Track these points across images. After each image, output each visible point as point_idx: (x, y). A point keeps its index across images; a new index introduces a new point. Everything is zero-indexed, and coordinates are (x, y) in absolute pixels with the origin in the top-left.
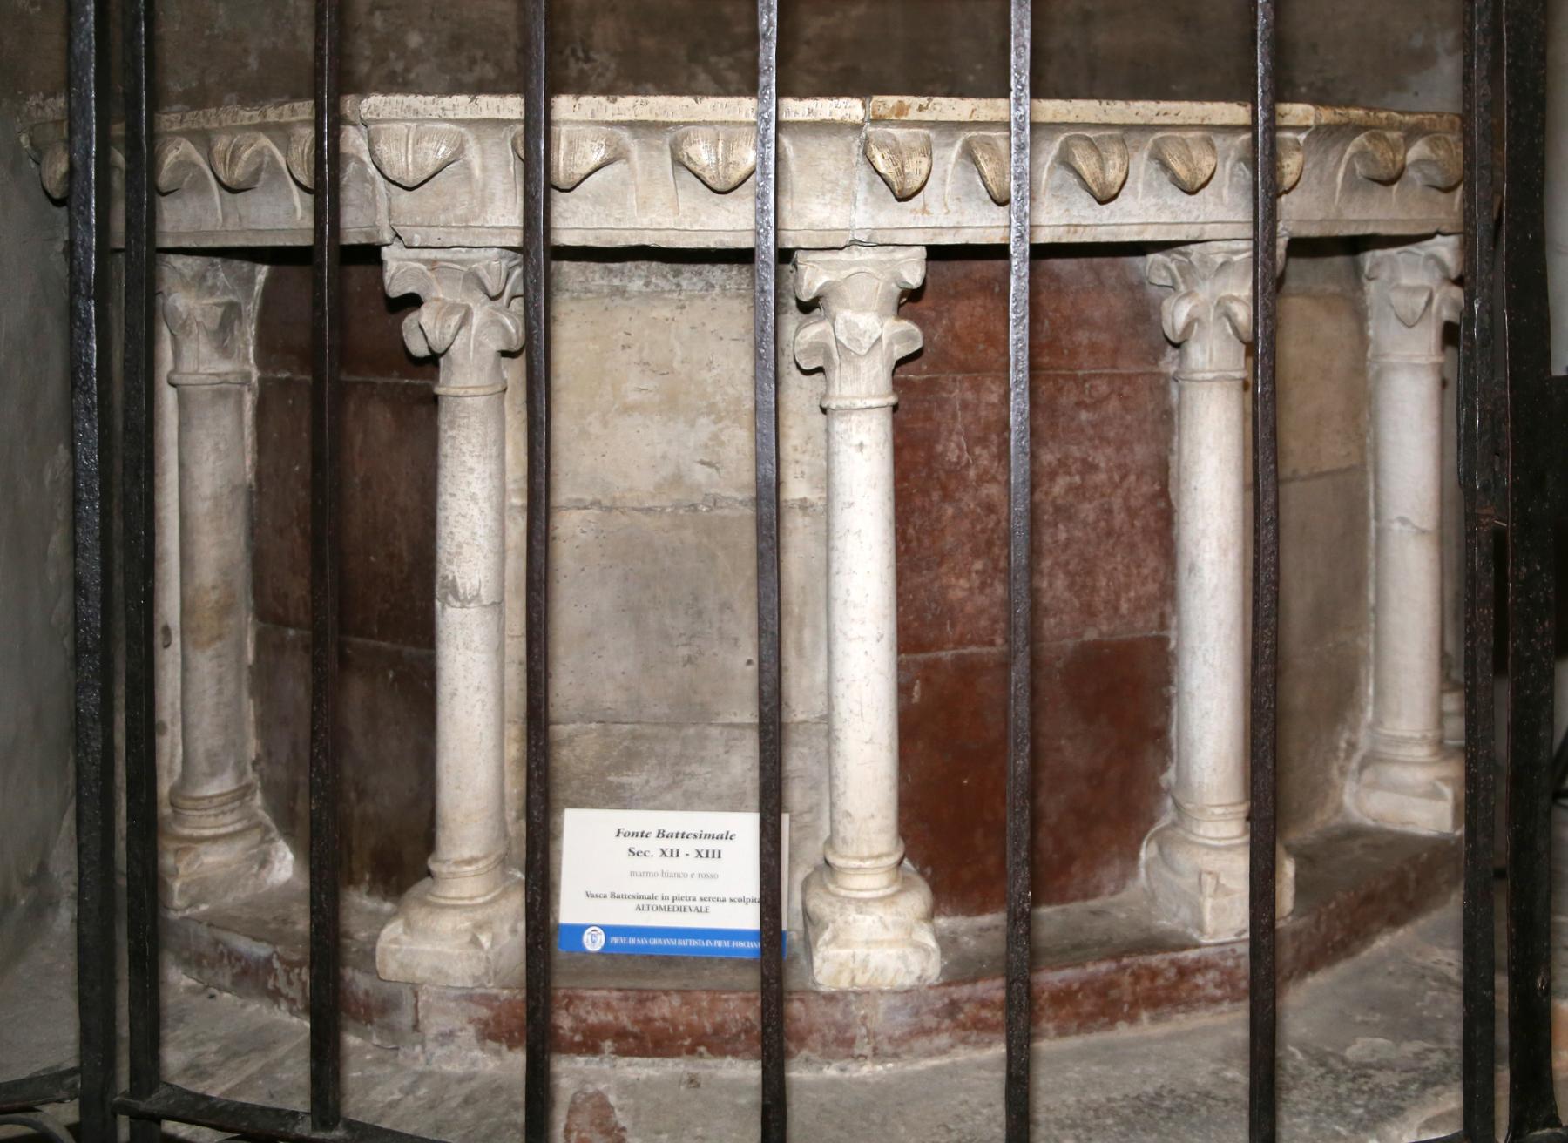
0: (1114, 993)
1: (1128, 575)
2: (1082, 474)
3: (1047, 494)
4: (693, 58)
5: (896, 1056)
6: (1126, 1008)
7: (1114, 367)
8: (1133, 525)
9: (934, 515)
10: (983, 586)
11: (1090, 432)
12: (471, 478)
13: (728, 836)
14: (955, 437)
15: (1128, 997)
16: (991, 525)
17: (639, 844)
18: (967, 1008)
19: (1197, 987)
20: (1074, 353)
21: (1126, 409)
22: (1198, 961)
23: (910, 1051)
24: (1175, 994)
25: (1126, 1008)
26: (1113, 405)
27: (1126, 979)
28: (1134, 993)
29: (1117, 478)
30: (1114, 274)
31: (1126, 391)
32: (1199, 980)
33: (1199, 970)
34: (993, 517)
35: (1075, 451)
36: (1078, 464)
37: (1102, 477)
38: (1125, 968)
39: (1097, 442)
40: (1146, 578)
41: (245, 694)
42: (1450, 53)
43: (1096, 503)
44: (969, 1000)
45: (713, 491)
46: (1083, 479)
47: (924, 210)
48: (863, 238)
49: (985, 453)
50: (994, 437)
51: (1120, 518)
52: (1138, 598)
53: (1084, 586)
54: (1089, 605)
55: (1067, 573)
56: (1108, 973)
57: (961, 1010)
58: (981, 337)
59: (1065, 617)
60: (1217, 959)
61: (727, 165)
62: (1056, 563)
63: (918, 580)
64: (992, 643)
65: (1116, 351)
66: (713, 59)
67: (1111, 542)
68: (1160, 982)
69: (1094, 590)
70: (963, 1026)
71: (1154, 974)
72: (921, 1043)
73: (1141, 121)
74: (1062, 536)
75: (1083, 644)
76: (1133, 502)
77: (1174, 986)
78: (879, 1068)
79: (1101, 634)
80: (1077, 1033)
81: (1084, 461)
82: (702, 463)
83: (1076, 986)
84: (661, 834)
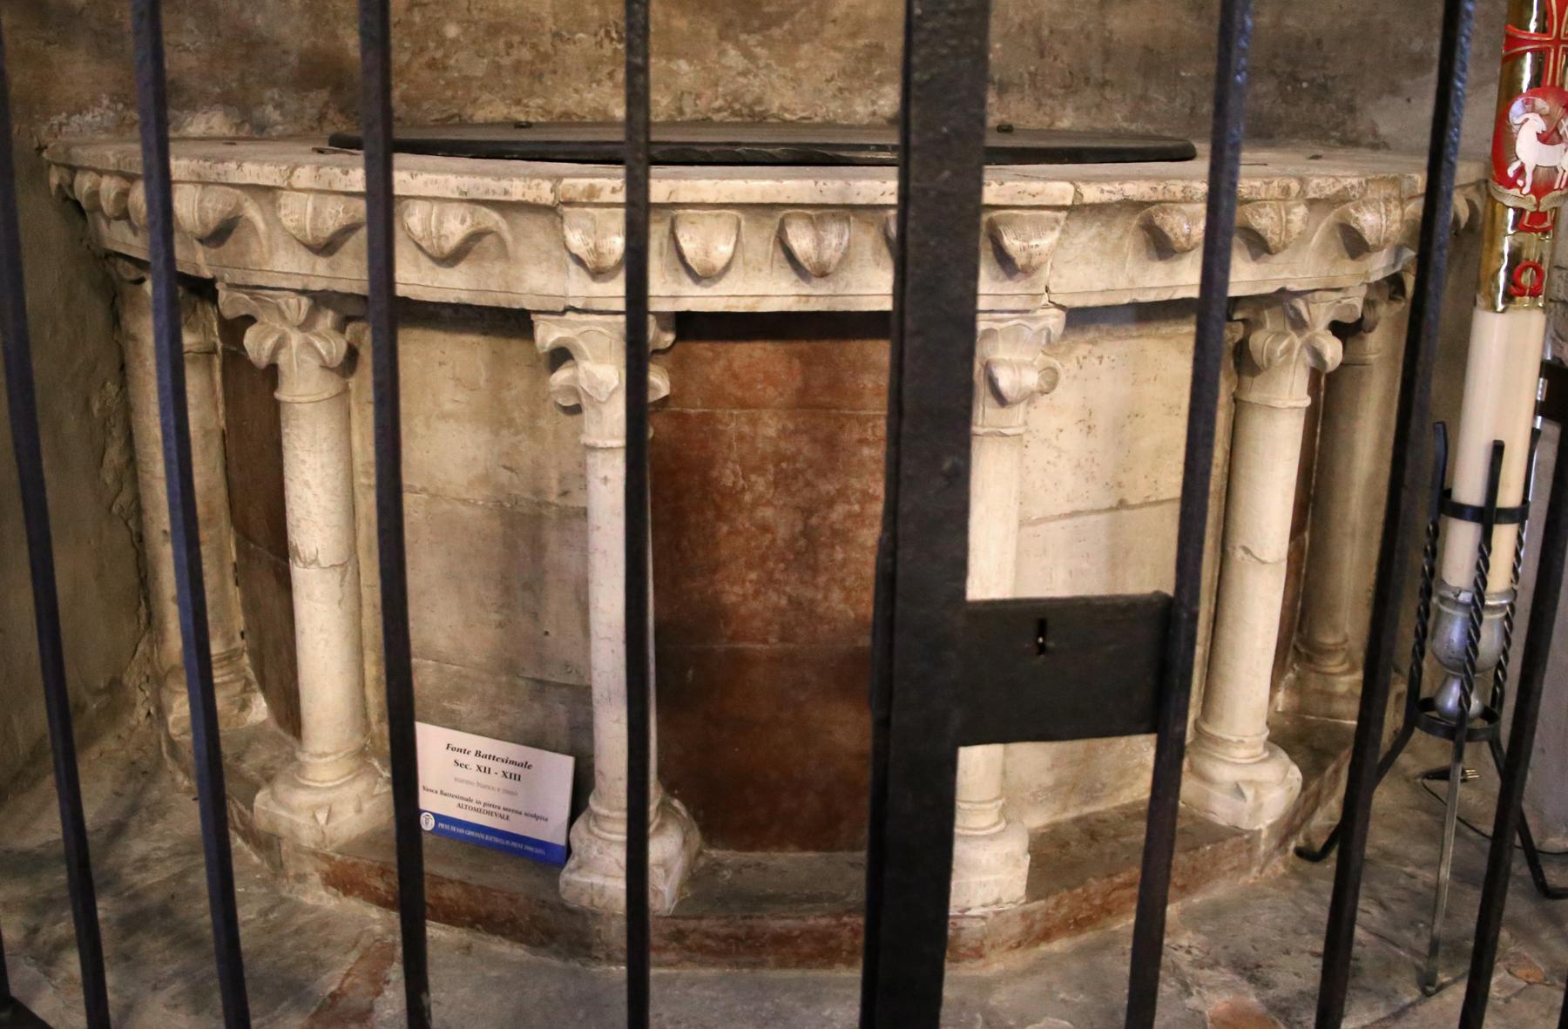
0: (833, 943)
2: (862, 503)
3: (824, 518)
4: (722, 36)
10: (757, 593)
12: (303, 468)
13: (527, 765)
14: (730, 465)
16: (766, 543)
17: (462, 758)
34: (769, 536)
35: (855, 483)
38: (845, 925)
41: (231, 583)
42: (325, 439)
44: (694, 931)
45: (515, 492)
46: (863, 508)
48: (579, 305)
49: (761, 481)
50: (771, 468)
55: (844, 588)
56: (827, 926)
58: (761, 376)
61: (440, 237)
64: (765, 641)
66: (743, 37)
70: (689, 949)
74: (839, 556)
80: (797, 967)
82: (505, 467)
83: (797, 933)
84: (478, 753)
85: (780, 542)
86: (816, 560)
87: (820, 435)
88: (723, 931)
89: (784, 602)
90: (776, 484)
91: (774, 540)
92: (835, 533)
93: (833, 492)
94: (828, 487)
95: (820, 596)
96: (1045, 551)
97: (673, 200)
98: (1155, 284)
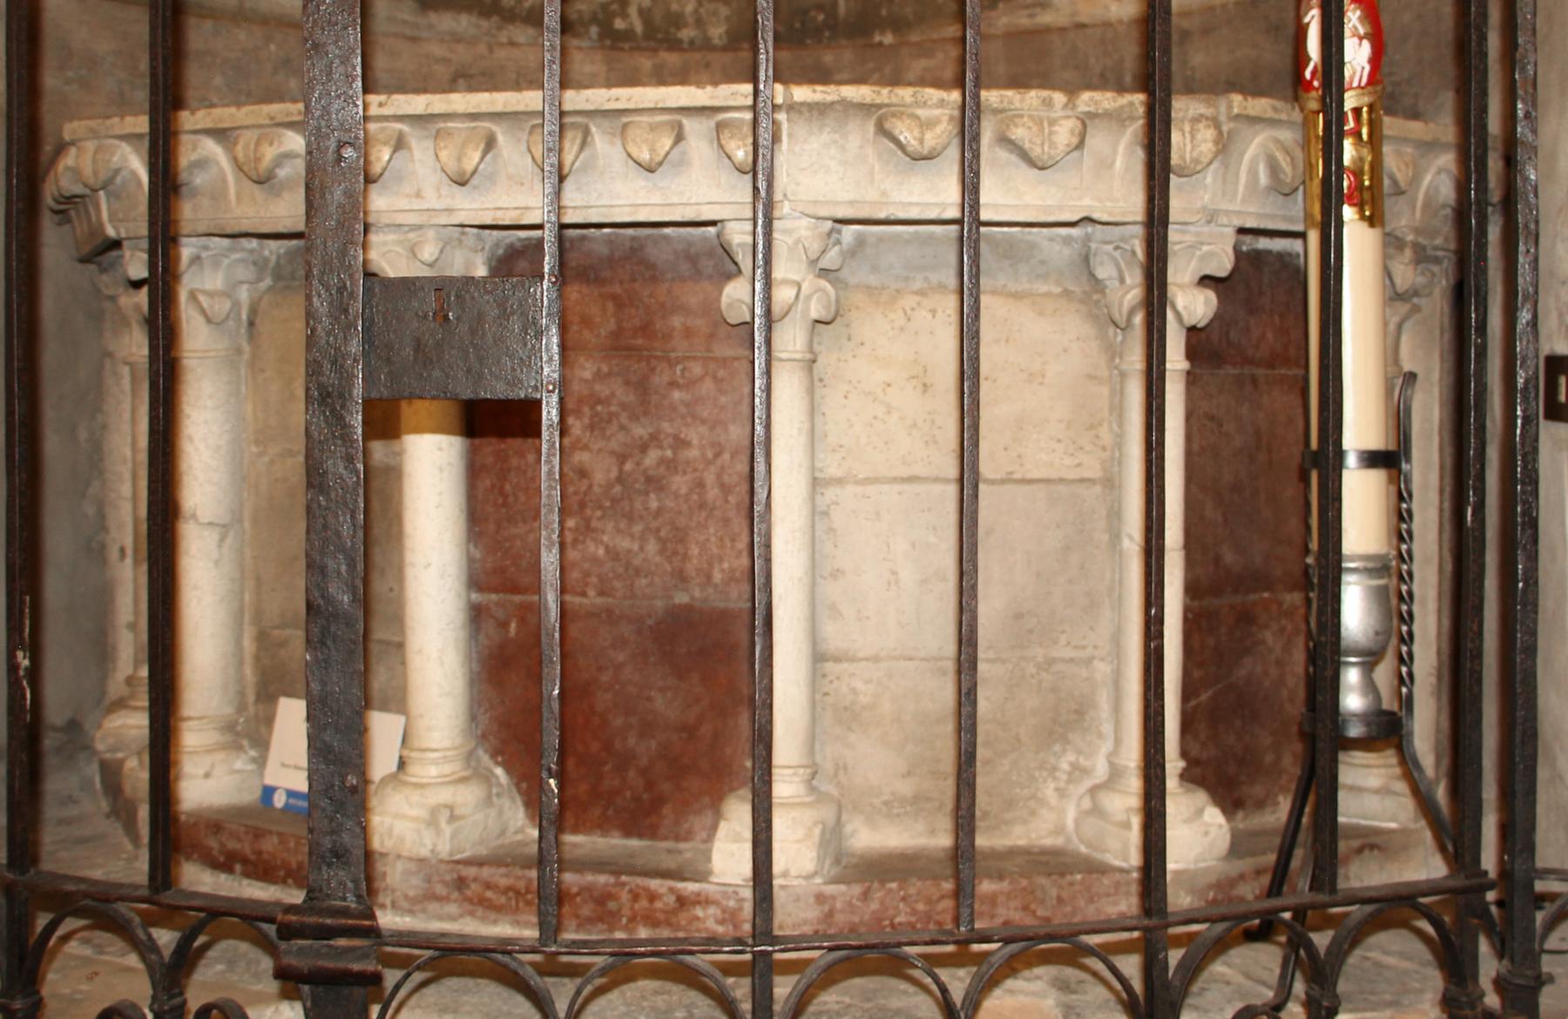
0: (612, 905)
1: (722, 547)
2: (675, 449)
3: (638, 464)
5: (411, 912)
6: (624, 920)
7: (708, 350)
8: (727, 501)
9: (529, 474)
11: (683, 410)
15: (626, 911)
16: (583, 489)
18: (473, 886)
19: (698, 918)
20: (668, 337)
21: (721, 392)
22: (699, 894)
23: (424, 911)
24: (674, 920)
25: (624, 920)
26: (707, 386)
27: (625, 896)
28: (632, 908)
29: (710, 455)
30: (711, 263)
31: (721, 373)
32: (699, 912)
33: (699, 903)
34: (586, 482)
36: (670, 440)
37: (693, 453)
38: (624, 884)
39: (689, 420)
40: (740, 552)
43: (688, 477)
44: (475, 880)
46: (675, 454)
47: (418, 195)
51: (713, 493)
52: (732, 570)
53: (675, 553)
54: (681, 571)
55: (659, 539)
56: (606, 885)
57: (468, 887)
59: (657, 579)
60: (718, 897)
62: (647, 529)
63: (514, 531)
64: (584, 594)
65: (712, 336)
67: (704, 514)
68: (658, 905)
69: (686, 557)
70: (470, 901)
71: (653, 897)
72: (433, 907)
73: (591, 107)
74: (654, 505)
75: (674, 606)
76: (726, 479)
77: (674, 912)
78: (398, 919)
79: (693, 598)
81: (676, 438)
85: (596, 489)
86: (632, 507)
87: (633, 378)
88: (503, 882)
89: (601, 552)
90: (592, 427)
91: (590, 486)
92: (649, 480)
93: (646, 437)
94: (640, 431)
95: (636, 547)
96: (878, 514)
97: (429, 111)
98: (914, 199)
